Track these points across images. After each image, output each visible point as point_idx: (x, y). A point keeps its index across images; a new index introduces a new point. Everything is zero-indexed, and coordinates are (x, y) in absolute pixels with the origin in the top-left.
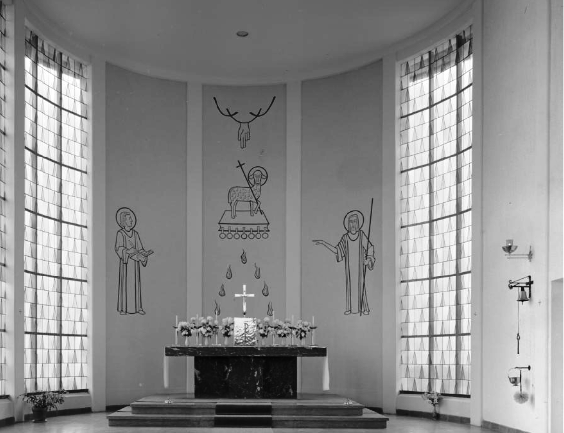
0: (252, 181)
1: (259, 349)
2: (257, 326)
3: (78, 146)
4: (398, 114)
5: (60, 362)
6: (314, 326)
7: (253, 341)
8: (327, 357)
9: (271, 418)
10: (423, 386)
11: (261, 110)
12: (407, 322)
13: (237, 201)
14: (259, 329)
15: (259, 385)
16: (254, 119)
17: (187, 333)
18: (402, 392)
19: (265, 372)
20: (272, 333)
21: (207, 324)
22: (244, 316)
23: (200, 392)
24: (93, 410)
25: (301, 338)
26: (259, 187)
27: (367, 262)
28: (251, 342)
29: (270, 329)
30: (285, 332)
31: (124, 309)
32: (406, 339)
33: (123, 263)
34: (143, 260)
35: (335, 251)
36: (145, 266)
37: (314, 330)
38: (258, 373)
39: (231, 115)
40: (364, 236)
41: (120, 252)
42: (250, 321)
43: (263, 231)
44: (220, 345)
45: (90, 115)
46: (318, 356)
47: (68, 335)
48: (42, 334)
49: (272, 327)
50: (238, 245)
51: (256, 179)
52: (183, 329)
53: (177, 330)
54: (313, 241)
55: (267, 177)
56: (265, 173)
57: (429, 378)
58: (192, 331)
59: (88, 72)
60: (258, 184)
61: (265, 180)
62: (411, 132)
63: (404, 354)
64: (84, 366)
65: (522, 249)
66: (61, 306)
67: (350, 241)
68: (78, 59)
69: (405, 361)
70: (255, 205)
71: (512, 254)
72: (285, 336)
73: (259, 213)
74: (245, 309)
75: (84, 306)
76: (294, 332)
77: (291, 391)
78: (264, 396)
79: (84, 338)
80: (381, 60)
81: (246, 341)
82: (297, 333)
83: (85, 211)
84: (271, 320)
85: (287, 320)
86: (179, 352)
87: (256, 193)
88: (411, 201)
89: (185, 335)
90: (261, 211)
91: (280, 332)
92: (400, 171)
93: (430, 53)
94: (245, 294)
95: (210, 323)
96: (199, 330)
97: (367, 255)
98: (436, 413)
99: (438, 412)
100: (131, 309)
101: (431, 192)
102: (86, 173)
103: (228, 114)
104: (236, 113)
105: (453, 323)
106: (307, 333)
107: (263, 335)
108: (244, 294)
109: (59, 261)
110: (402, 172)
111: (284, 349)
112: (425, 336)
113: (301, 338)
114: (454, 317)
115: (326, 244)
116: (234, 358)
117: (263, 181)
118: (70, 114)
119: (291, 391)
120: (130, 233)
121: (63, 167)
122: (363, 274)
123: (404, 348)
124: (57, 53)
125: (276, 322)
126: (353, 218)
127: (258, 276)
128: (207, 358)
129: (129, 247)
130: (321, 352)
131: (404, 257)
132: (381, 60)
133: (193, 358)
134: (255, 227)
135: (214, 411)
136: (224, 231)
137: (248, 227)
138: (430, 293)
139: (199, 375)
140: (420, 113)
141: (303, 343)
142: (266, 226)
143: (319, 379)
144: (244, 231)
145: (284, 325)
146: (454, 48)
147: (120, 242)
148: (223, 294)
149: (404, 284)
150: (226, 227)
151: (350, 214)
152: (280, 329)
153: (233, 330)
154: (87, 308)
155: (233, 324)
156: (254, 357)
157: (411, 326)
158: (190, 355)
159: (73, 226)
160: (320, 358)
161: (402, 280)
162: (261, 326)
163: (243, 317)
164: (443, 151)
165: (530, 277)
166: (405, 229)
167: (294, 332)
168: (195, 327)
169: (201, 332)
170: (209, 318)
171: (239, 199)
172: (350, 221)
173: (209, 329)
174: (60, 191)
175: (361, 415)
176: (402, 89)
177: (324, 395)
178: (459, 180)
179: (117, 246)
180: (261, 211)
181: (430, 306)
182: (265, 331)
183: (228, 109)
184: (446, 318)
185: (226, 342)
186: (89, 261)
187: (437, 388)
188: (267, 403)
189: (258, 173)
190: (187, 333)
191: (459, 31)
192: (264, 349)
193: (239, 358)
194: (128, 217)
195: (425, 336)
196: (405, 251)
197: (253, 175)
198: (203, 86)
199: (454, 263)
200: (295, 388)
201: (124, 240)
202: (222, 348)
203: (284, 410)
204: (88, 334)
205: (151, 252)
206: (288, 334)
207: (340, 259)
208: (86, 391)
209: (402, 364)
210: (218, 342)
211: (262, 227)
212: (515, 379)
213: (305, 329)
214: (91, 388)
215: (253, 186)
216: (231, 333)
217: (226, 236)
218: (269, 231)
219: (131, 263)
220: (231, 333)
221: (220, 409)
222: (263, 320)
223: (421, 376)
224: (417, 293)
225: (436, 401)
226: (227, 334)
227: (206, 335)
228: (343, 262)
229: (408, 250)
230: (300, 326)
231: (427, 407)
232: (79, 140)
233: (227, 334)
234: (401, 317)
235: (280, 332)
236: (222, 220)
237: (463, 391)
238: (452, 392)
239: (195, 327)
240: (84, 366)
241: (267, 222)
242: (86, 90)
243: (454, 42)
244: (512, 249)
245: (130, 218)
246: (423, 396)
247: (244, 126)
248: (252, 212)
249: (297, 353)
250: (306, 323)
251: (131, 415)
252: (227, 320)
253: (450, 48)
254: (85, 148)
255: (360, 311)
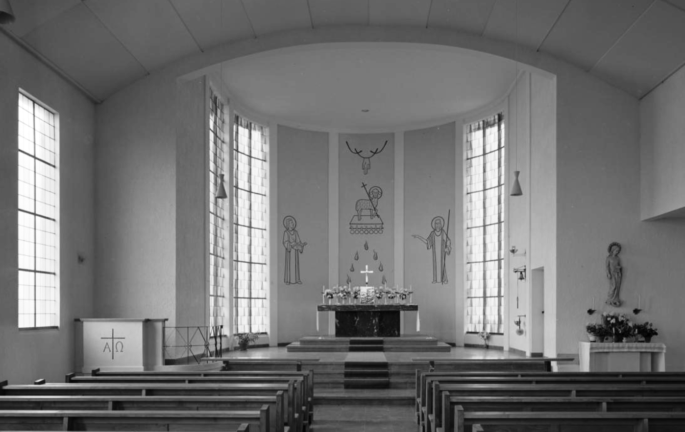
0: (372, 196)
1: (376, 306)
2: (375, 291)
3: (260, 179)
4: (465, 158)
5: (250, 315)
6: (411, 291)
7: (373, 301)
8: (418, 312)
9: (382, 347)
10: (480, 329)
11: (377, 149)
12: (471, 288)
13: (362, 209)
14: (376, 293)
15: (376, 329)
16: (373, 155)
17: (330, 297)
18: (468, 332)
19: (380, 320)
20: (384, 296)
21: (344, 290)
22: (367, 285)
23: (339, 333)
24: (270, 345)
25: (403, 299)
26: (376, 199)
27: (446, 250)
28: (371, 302)
29: (383, 293)
30: (393, 295)
31: (289, 281)
32: (470, 299)
33: (288, 251)
34: (300, 249)
35: (426, 242)
36: (301, 253)
37: (411, 294)
38: (375, 321)
39: (358, 153)
40: (444, 234)
41: (286, 245)
42: (371, 289)
43: (380, 229)
44: (352, 304)
45: (268, 159)
46: (413, 310)
47: (255, 298)
48: (241, 298)
49: (384, 292)
50: (361, 238)
51: (374, 195)
52: (328, 294)
53: (323, 295)
54: (413, 236)
55: (382, 194)
56: (380, 191)
57: (484, 324)
58: (334, 295)
59: (267, 131)
60: (375, 198)
61: (380, 196)
62: (473, 169)
63: (469, 309)
64: (264, 317)
65: (520, 251)
66: (251, 281)
67: (436, 237)
68: (261, 125)
69: (469, 313)
70: (374, 211)
71: (516, 253)
72: (392, 298)
73: (376, 216)
74: (367, 281)
75: (264, 280)
76: (398, 295)
77: (396, 332)
78: (379, 336)
79: (264, 300)
80: (454, 122)
81: (367, 301)
82: (400, 296)
83: (264, 219)
84: (384, 288)
85: (394, 288)
86: (326, 308)
87: (375, 205)
88: (473, 212)
89: (329, 298)
90: (378, 216)
91: (389, 295)
92: (466, 193)
93: (483, 121)
94: (367, 271)
95: (346, 290)
96: (339, 294)
97: (446, 246)
98: (486, 345)
99: (487, 344)
100: (293, 281)
101: (484, 208)
102: (265, 195)
103: (355, 152)
104: (361, 151)
105: (496, 290)
106: (407, 296)
107: (379, 298)
108: (367, 271)
109: (250, 252)
110: (468, 194)
111: (391, 306)
112: (489, 297)
113: (403, 299)
114: (497, 286)
115: (421, 238)
116: (360, 312)
117: (379, 196)
118: (256, 160)
119: (396, 332)
120: (292, 233)
121: (252, 194)
122: (443, 258)
123: (469, 304)
124: (249, 123)
125: (387, 289)
126: (438, 222)
127: (376, 258)
128: (343, 312)
129: (291, 241)
130: (415, 308)
131: (469, 247)
132: (454, 122)
133: (334, 313)
134: (373, 226)
135: (349, 343)
136: (355, 229)
137: (369, 226)
138: (484, 271)
139: (338, 323)
140: (478, 158)
141: (403, 302)
142: (381, 225)
143: (414, 325)
144: (366, 229)
145: (392, 291)
146: (497, 121)
147: (286, 239)
148: (352, 270)
149: (469, 265)
150: (354, 226)
151: (436, 219)
152: (390, 293)
153: (359, 294)
154: (266, 281)
155: (360, 290)
156: (373, 312)
157: (473, 291)
158: (333, 310)
159: (258, 230)
160: (415, 312)
161: (468, 262)
162: (377, 292)
163: (365, 286)
164: (491, 184)
165: (525, 266)
166: (469, 230)
167: (398, 295)
168: (336, 293)
169: (340, 296)
170: (345, 287)
171: (363, 208)
172: (435, 223)
173: (345, 294)
174: (250, 209)
175: (436, 344)
176: (467, 141)
177: (418, 335)
178: (499, 203)
179: (284, 241)
180: (378, 216)
181: (484, 279)
182: (380, 295)
183: (355, 149)
184: (492, 286)
185: (355, 302)
186: (267, 251)
187: (488, 330)
188: (381, 338)
189: (376, 191)
190: (330, 297)
191: (499, 112)
192: (379, 306)
193: (363, 312)
194: (291, 222)
195: (489, 297)
196: (469, 244)
197: (372, 191)
198: (339, 134)
199: (497, 253)
200: (399, 330)
201: (289, 237)
202: (353, 306)
203: (391, 342)
204: (267, 297)
205: (305, 244)
206: (395, 297)
207: (429, 247)
208: (266, 333)
209: (468, 315)
210: (351, 302)
211: (378, 226)
212: (518, 322)
213: (406, 294)
214: (268, 331)
215: (372, 199)
216: (358, 296)
217: (355, 232)
218: (383, 228)
219: (293, 251)
220: (358, 296)
221: (352, 342)
222: (378, 288)
223: (479, 323)
224: (477, 270)
225: (485, 337)
226: (356, 297)
227: (343, 298)
228: (431, 249)
229: (472, 243)
230: (402, 292)
231: (481, 342)
232: (261, 175)
233: (356, 297)
234: (467, 286)
235: (389, 295)
236: (353, 220)
237: (502, 331)
238: (496, 331)
239: (336, 293)
240: (264, 317)
241: (381, 222)
242: (265, 143)
243: (497, 117)
244: (515, 251)
245: (292, 223)
246: (479, 334)
247: (367, 161)
248: (372, 216)
249: (399, 308)
250: (406, 290)
251: (299, 345)
252: (356, 288)
253: (494, 120)
254: (264, 179)
255: (442, 281)
